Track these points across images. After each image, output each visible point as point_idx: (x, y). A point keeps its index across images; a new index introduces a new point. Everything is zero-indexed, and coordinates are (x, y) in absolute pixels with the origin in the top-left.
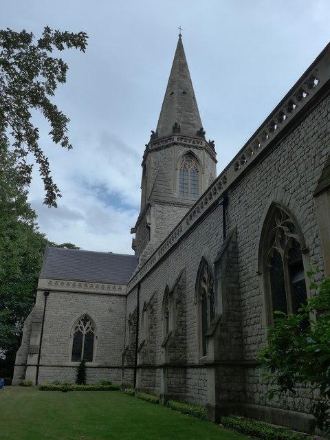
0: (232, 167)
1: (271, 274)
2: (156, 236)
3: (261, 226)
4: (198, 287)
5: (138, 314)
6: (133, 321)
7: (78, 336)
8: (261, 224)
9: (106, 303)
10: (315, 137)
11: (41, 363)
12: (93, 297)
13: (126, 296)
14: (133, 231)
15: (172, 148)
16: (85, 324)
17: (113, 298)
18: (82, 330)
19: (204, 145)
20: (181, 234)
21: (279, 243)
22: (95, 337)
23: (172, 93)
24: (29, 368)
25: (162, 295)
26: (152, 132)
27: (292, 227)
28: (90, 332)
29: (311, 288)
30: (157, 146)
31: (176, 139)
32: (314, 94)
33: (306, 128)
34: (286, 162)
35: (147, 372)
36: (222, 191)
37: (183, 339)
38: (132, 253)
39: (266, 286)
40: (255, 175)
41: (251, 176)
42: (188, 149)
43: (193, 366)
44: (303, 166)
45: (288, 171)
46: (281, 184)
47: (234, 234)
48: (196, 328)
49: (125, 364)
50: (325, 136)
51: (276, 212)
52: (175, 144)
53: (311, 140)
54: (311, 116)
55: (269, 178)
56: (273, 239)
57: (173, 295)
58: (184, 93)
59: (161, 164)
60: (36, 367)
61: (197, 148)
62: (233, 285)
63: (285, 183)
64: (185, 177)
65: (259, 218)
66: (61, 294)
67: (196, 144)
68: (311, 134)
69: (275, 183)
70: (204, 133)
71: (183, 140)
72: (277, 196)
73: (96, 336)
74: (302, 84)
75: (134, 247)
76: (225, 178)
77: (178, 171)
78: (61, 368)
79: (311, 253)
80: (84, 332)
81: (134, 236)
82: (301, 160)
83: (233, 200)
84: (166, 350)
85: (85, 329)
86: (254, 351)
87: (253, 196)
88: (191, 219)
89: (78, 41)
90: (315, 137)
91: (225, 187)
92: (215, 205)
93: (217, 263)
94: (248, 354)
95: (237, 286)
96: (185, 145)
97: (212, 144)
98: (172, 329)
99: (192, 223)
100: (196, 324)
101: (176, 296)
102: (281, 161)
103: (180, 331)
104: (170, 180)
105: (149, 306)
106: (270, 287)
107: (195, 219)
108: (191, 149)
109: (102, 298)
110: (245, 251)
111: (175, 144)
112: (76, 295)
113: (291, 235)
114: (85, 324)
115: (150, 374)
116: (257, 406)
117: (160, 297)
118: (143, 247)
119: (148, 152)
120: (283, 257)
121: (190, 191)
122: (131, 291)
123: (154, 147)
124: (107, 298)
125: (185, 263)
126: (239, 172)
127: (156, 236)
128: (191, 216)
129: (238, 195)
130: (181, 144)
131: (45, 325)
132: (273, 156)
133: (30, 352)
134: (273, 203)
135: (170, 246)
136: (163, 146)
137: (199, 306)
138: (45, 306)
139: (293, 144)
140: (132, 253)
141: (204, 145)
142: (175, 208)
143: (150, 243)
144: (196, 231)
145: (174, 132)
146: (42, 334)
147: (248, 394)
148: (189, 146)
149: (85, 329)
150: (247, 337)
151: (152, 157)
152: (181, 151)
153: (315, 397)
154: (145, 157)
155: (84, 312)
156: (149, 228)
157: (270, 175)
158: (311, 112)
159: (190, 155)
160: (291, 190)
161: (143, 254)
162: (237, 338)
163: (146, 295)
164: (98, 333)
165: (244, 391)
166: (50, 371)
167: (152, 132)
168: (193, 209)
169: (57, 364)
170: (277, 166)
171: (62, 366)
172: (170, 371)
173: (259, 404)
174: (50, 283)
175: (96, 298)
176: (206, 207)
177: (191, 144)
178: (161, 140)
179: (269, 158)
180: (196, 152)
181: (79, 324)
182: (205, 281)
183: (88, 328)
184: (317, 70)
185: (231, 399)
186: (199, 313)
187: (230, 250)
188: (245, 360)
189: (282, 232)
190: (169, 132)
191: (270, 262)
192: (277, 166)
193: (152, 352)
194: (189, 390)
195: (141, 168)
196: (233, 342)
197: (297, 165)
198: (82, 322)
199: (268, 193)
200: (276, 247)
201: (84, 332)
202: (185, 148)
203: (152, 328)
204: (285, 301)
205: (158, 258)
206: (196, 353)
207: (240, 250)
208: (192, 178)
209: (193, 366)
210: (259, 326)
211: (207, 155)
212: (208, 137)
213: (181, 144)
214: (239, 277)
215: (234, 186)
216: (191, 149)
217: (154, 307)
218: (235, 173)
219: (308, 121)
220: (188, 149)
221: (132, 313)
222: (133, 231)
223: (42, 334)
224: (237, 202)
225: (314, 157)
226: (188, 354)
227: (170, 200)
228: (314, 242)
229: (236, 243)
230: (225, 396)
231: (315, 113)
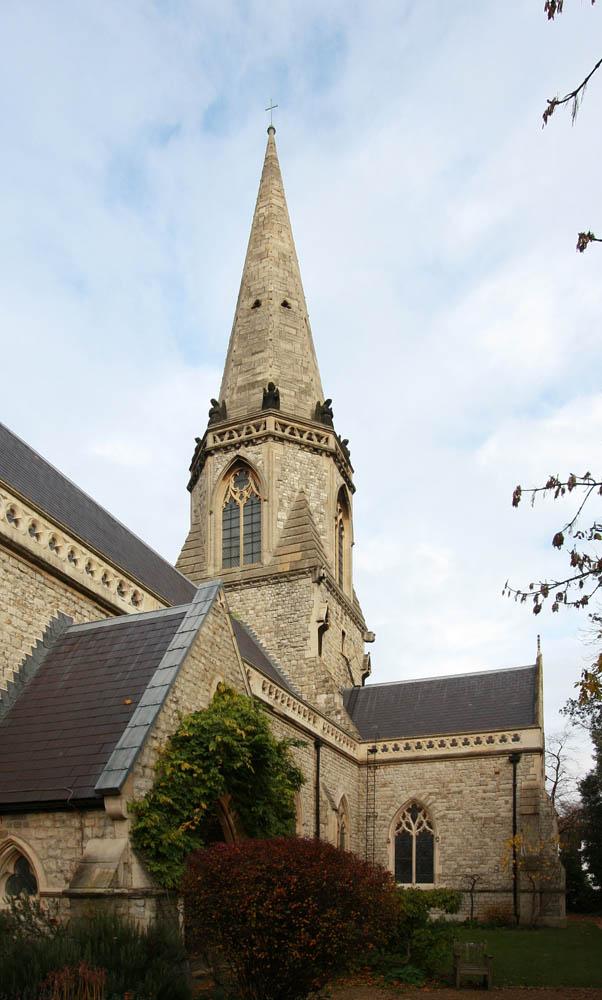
11: (511, 895)
18: (411, 829)
42: (231, 455)
67: (315, 442)
80: (414, 832)
123: (219, 442)
198: (409, 816)
201: (414, 832)
220: (231, 455)
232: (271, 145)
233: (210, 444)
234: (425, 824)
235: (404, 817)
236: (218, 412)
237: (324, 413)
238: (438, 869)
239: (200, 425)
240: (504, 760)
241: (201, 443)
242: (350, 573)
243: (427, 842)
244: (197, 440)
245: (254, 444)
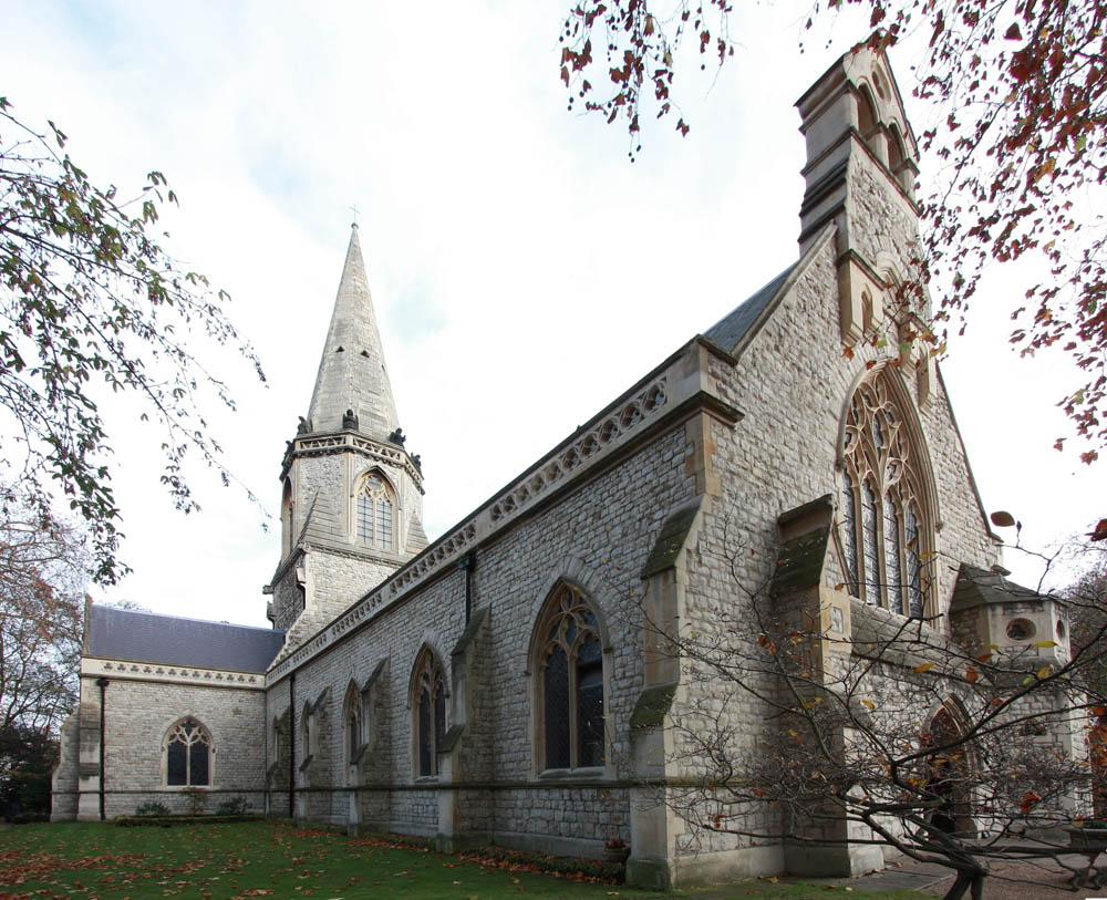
0: (487, 513)
1: (546, 675)
2: (315, 603)
3: (537, 610)
4: (414, 684)
5: (293, 718)
6: (283, 729)
7: (176, 752)
8: (536, 607)
9: (229, 701)
10: (645, 489)
11: (106, 789)
12: (197, 691)
13: (264, 691)
14: (267, 590)
15: (343, 456)
16: (189, 732)
17: (240, 694)
18: (185, 740)
19: (403, 459)
20: (380, 607)
21: (563, 635)
22: (210, 750)
23: (341, 350)
24: (83, 796)
25: (343, 693)
26: (301, 418)
27: (587, 616)
28: (200, 742)
29: (610, 698)
30: (311, 448)
31: (350, 441)
32: (655, 420)
33: (632, 472)
34: (590, 520)
35: (317, 797)
36: (464, 549)
37: (385, 754)
38: (269, 625)
39: (537, 690)
40: (530, 535)
41: (523, 532)
42: (375, 463)
43: (404, 788)
44: (618, 530)
45: (592, 534)
46: (576, 552)
47: (487, 615)
48: (411, 740)
49: (273, 787)
50: (663, 491)
51: (563, 591)
52: (348, 449)
53: (639, 493)
54: (643, 455)
55: (556, 540)
56: (555, 629)
57: (368, 695)
58: (364, 354)
59: (322, 483)
60: (98, 795)
61: (390, 463)
62: (482, 687)
63: (584, 551)
64: (367, 512)
65: (534, 598)
66: (135, 686)
67: (388, 457)
68: (639, 483)
69: (565, 548)
70: (403, 439)
71: (365, 445)
72: (571, 568)
73: (212, 747)
74: (633, 399)
75: (270, 617)
76: (472, 528)
77: (355, 499)
78: (149, 795)
79: (617, 653)
80: (189, 743)
81: (270, 598)
82: (616, 521)
83: (486, 565)
84: (358, 768)
85: (189, 739)
86: (512, 770)
87: (525, 564)
88: (401, 585)
89: (165, 182)
90: (645, 489)
91: (469, 544)
92: (449, 570)
93: (458, 654)
94: (502, 774)
95: (489, 688)
96: (367, 455)
97: (416, 461)
98: (367, 741)
99: (401, 592)
100: (411, 735)
101: (374, 696)
102: (581, 518)
103: (381, 744)
104: (339, 513)
105: (317, 708)
106: (543, 692)
107: (408, 587)
108: (380, 464)
109: (220, 693)
110: (505, 642)
111: (348, 449)
112: (166, 688)
113: (585, 627)
114: (189, 732)
115: (323, 799)
116: (512, 834)
117: (339, 694)
118: (292, 618)
119: (291, 455)
120: (569, 655)
121: (377, 536)
122: (273, 686)
123: (306, 448)
124: (229, 694)
125: (397, 647)
126: (501, 523)
127: (315, 603)
128: (401, 580)
129: (496, 558)
130: (359, 452)
131: (106, 732)
132: (567, 507)
133: (84, 772)
134: (561, 580)
135: (357, 623)
136: (325, 451)
137: (415, 709)
138: (103, 703)
139: (606, 494)
140: (269, 625)
141: (403, 459)
142: (349, 561)
143: (305, 612)
144: (411, 605)
145: (345, 427)
146: (102, 746)
147: (498, 820)
148: (375, 458)
149: (189, 739)
150: (499, 753)
151: (302, 467)
152: (359, 464)
153: (601, 821)
154: (287, 466)
155: (187, 713)
156: (303, 589)
157: (559, 534)
158: (645, 448)
159: (377, 473)
160: (595, 563)
161: (293, 628)
162: (485, 755)
163: (308, 690)
164: (215, 744)
165: (493, 817)
166: (130, 799)
167: (301, 418)
168: (404, 572)
169: (140, 788)
170: (572, 524)
171: (150, 792)
172: (366, 794)
173: (515, 831)
174: (108, 667)
175: (208, 692)
176: (432, 570)
177: (379, 454)
178: (318, 439)
179: (559, 509)
180: (386, 469)
181: (178, 730)
182: (426, 677)
183: (195, 737)
184: (665, 379)
185: (475, 826)
186: (414, 720)
187: (477, 633)
188: (496, 782)
189: (571, 619)
190: (335, 425)
191: (548, 661)
192: (572, 524)
193: (325, 770)
194: (397, 817)
195: (280, 486)
196: (480, 759)
197: (609, 527)
198: (183, 730)
199: (552, 563)
200: (559, 642)
201: (189, 743)
202: (368, 461)
203: (324, 738)
204: (567, 715)
205: (330, 639)
206: (411, 772)
207: (495, 639)
208: (381, 515)
209: (404, 788)
210: (522, 741)
211: (407, 478)
212: (410, 447)
213: (359, 452)
214: (491, 676)
215: (488, 543)
216: (380, 464)
217: (327, 710)
218: (493, 524)
219: (636, 463)
220: (375, 463)
221: (279, 716)
222: (267, 590)
223: (102, 746)
224: (494, 568)
225: (640, 520)
226: (395, 774)
227: (338, 546)
228: (624, 639)
229: (490, 629)
230: (466, 823)
231: (651, 451)
232: (354, 235)
233: (298, 448)
234: (178, 736)
235: (178, 730)
236: (304, 426)
237: (397, 438)
238: (212, 771)
239: (292, 434)
240: (93, 682)
241: (291, 446)
242: (283, 543)
243: (201, 751)
244: (288, 442)
245: (336, 453)
